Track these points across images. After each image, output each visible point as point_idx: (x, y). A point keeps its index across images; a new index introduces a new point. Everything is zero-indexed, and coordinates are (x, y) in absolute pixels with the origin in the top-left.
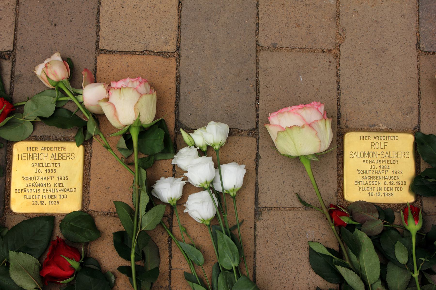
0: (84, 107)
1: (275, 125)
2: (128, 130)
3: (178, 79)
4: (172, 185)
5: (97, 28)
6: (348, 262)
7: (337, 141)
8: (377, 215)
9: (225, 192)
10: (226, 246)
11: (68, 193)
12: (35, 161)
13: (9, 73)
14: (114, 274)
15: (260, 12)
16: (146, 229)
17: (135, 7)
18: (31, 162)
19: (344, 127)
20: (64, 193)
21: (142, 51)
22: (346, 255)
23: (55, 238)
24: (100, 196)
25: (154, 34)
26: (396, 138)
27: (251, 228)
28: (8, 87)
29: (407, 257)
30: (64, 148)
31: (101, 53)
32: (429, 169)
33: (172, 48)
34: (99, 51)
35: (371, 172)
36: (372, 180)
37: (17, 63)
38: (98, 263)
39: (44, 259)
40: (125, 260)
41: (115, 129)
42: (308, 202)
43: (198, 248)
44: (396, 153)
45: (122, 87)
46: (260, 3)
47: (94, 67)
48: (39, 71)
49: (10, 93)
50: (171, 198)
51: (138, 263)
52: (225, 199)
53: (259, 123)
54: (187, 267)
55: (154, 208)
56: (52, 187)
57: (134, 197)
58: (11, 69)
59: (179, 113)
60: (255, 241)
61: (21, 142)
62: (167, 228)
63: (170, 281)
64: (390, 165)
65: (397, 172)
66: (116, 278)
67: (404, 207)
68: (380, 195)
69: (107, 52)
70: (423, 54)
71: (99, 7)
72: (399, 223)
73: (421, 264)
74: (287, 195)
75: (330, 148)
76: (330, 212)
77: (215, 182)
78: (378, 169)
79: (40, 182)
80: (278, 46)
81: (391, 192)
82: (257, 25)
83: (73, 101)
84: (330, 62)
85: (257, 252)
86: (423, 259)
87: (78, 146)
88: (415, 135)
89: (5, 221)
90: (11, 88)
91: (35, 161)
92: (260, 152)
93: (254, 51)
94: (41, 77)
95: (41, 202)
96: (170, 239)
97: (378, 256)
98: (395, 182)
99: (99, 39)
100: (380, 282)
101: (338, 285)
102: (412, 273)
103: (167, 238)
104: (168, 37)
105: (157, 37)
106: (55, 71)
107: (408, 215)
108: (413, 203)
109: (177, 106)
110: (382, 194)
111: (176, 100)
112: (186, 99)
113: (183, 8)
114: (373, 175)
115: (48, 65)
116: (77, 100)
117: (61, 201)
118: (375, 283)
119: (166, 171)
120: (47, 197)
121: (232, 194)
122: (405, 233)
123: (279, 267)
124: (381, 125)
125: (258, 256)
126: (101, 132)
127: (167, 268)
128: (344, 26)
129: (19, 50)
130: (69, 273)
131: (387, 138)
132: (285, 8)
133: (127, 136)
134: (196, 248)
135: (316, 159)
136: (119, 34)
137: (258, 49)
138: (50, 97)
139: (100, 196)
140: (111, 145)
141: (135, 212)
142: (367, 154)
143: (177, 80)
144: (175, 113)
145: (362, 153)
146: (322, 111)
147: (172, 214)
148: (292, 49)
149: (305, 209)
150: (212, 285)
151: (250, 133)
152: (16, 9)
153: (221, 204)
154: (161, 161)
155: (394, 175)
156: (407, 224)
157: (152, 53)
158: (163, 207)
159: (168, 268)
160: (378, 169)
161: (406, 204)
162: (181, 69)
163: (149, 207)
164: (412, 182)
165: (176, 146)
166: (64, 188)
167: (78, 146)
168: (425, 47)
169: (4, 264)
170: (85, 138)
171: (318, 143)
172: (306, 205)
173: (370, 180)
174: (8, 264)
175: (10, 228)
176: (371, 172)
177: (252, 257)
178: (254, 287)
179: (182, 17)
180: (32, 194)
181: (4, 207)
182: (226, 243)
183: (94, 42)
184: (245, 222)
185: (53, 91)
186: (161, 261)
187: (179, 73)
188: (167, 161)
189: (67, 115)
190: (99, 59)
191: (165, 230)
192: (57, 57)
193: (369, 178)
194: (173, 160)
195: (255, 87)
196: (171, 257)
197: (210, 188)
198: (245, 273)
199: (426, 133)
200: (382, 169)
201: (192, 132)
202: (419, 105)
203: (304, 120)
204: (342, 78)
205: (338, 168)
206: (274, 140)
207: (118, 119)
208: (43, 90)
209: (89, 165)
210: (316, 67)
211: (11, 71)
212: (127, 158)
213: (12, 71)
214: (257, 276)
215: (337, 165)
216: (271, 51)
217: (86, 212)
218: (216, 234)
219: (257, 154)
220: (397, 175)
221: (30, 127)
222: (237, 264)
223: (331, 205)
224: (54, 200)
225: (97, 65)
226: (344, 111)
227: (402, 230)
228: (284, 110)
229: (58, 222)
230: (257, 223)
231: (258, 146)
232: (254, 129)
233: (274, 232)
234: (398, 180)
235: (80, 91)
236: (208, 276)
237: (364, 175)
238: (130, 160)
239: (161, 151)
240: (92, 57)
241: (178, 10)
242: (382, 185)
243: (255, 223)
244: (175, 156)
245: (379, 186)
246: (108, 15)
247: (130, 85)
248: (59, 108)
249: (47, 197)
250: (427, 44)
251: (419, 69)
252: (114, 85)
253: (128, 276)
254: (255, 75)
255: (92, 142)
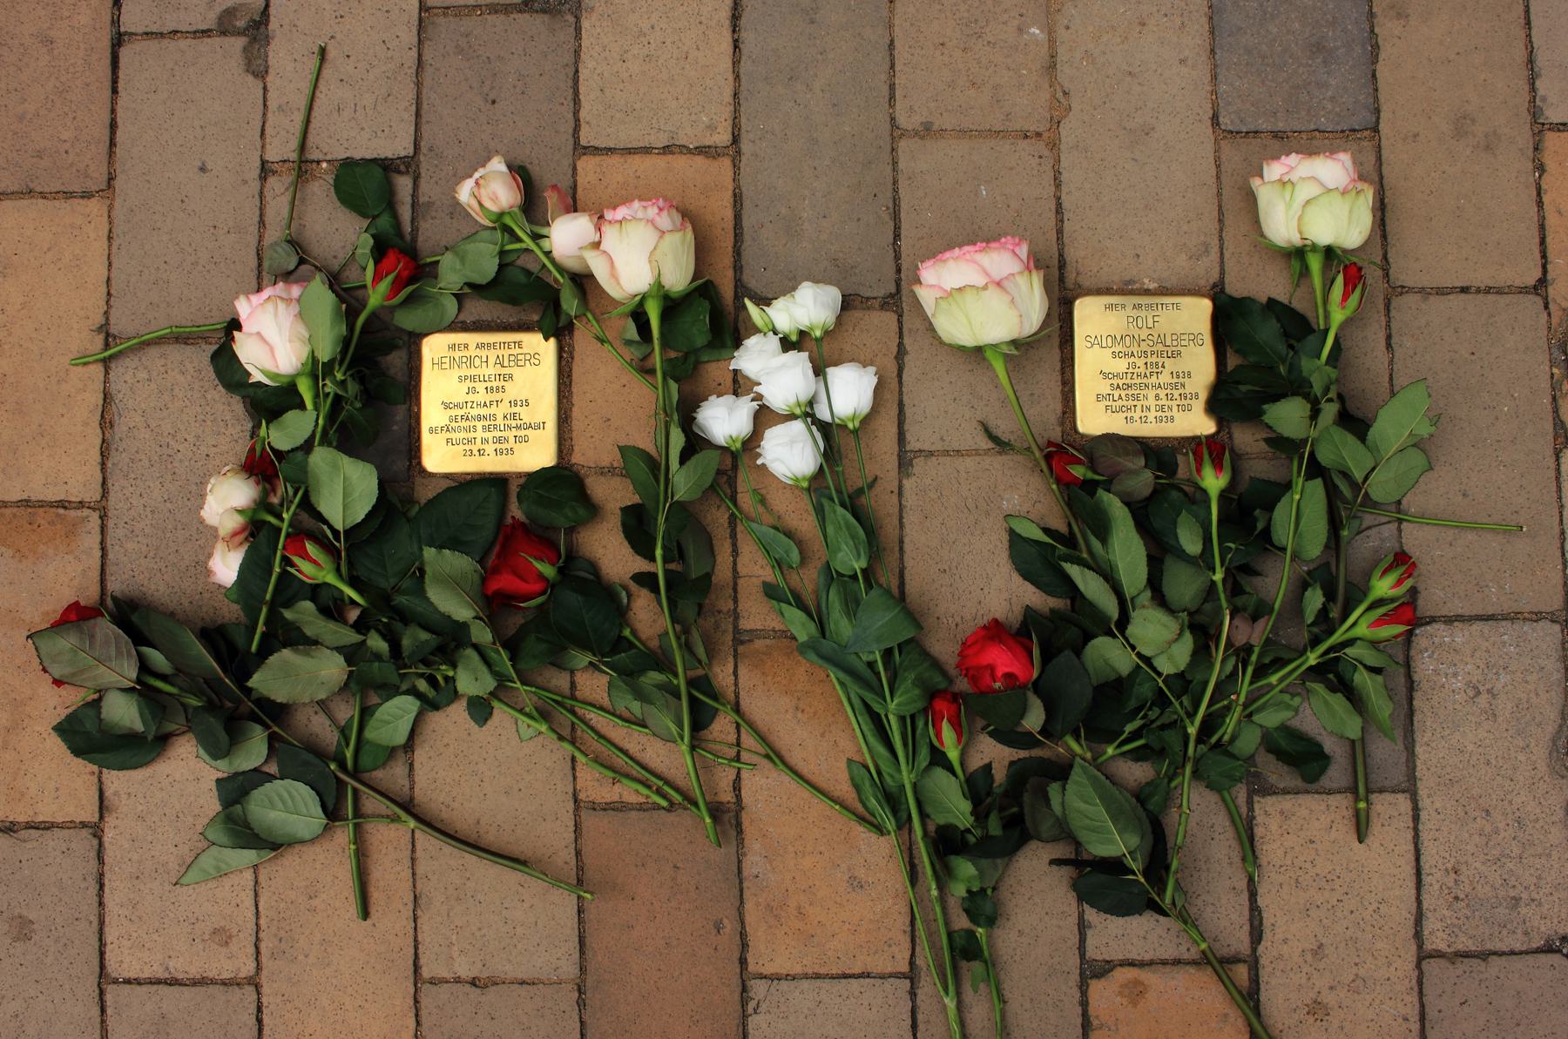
0: (553, 261)
1: (931, 286)
2: (641, 303)
3: (737, 199)
4: (731, 410)
5: (575, 104)
6: (1085, 555)
7: (1060, 315)
8: (1142, 462)
9: (837, 421)
10: (841, 528)
11: (529, 432)
12: (465, 371)
13: (409, 200)
14: (625, 588)
15: (897, 62)
16: (682, 499)
17: (647, 59)
18: (456, 373)
19: (1072, 287)
20: (522, 433)
21: (664, 148)
22: (1081, 541)
23: (509, 521)
24: (592, 437)
25: (687, 112)
26: (1177, 306)
27: (892, 492)
28: (407, 228)
29: (1201, 543)
30: (519, 344)
31: (584, 154)
32: (1241, 365)
33: (722, 137)
34: (580, 150)
35: (1129, 376)
36: (1130, 392)
37: (422, 180)
38: (594, 568)
39: (490, 562)
40: (647, 562)
41: (615, 303)
42: (1004, 438)
43: (789, 534)
44: (1177, 337)
45: (624, 217)
46: (896, 43)
47: (571, 183)
48: (464, 193)
49: (412, 239)
50: (731, 437)
51: (672, 566)
52: (839, 438)
53: (903, 283)
54: (768, 570)
55: (697, 456)
56: (500, 421)
57: (658, 437)
58: (411, 192)
59: (742, 267)
60: (901, 518)
61: (437, 335)
62: (725, 495)
63: (736, 601)
64: (1166, 360)
65: (1181, 375)
66: (629, 595)
67: (1195, 444)
68: (1148, 421)
69: (596, 151)
70: (1225, 137)
71: (576, 63)
72: (1185, 477)
73: (1230, 556)
74: (963, 425)
75: (1042, 328)
76: (1048, 458)
77: (817, 403)
78: (1142, 370)
79: (475, 412)
80: (935, 127)
81: (1169, 414)
82: (892, 87)
83: (532, 251)
84: (1040, 157)
85: (906, 540)
86: (1232, 545)
87: (546, 339)
88: (1214, 300)
89: (413, 489)
90: (412, 230)
91: (465, 371)
92: (907, 341)
93: (888, 139)
94: (469, 206)
95: (479, 451)
96: (732, 516)
97: (1142, 542)
98: (1176, 394)
99: (580, 126)
100: (1148, 594)
101: (1069, 602)
102: (1211, 573)
103: (727, 516)
104: (714, 117)
105: (693, 117)
106: (494, 193)
107: (1202, 460)
108: (1213, 435)
109: (737, 253)
110: (1151, 418)
111: (736, 242)
112: (754, 240)
113: (744, 58)
114: (1133, 382)
115: (481, 182)
116: (541, 248)
117: (517, 447)
118: (1139, 594)
119: (720, 384)
120: (490, 441)
121: (851, 426)
122: (1198, 495)
123: (950, 569)
124: (1146, 281)
125: (907, 547)
126: (587, 309)
127: (729, 574)
128: (1067, 86)
129: (425, 155)
130: (538, 587)
131: (1160, 306)
132: (946, 52)
133: (639, 316)
134: (785, 534)
135: (1015, 352)
136: (618, 115)
137: (895, 134)
138: (488, 245)
139: (592, 437)
140: (610, 335)
141: (660, 464)
142: (1119, 338)
143: (735, 201)
144: (734, 267)
145: (1109, 338)
146: (1024, 255)
147: (735, 467)
148: (963, 133)
149: (1000, 453)
150: (818, 607)
151: (885, 303)
152: (417, 74)
153: (830, 446)
154: (709, 364)
155: (1175, 380)
156: (1200, 476)
157: (684, 150)
158: (715, 454)
159: (731, 575)
160: (1142, 370)
161: (1199, 437)
162: (745, 180)
163: (685, 457)
164: (1209, 393)
165: (739, 334)
166: (522, 422)
167: (546, 339)
168: (1228, 122)
169: (414, 572)
170: (558, 321)
171: (1016, 320)
172: (1000, 445)
173: (1126, 392)
174: (422, 571)
175: (423, 501)
176: (1129, 376)
177: (897, 549)
178: (899, 608)
179: (742, 76)
180: (462, 435)
181: (411, 462)
182: (842, 522)
183: (571, 131)
184: (879, 481)
185: (494, 232)
186: (718, 562)
187: (739, 187)
188: (722, 364)
189: (522, 279)
190: (580, 164)
191: (722, 499)
192: (497, 165)
193: (1125, 387)
194: (733, 361)
195: (891, 210)
196: (735, 552)
197: (807, 415)
198: (883, 580)
199: (1237, 295)
200: (1150, 370)
201: (768, 305)
202: (1221, 239)
203: (987, 274)
204: (1064, 189)
205: (1062, 369)
206: (930, 316)
207: (619, 284)
208: (473, 231)
209: (570, 376)
210: (1011, 169)
211: (413, 196)
212: (642, 360)
213: (415, 195)
214: (907, 587)
215: (1059, 364)
216: (922, 138)
217: (566, 468)
218: (822, 506)
219: (900, 345)
220: (1181, 380)
221: (451, 306)
222: (863, 563)
223: (1050, 444)
224: (504, 446)
225: (578, 178)
226: (1071, 254)
227: (1193, 489)
228: (948, 255)
229: (514, 489)
230: (905, 482)
231: (901, 329)
232: (892, 296)
233: (939, 498)
234: (1182, 391)
235: (544, 231)
236: (810, 590)
237: (1115, 382)
238: (648, 364)
239: (706, 343)
240: (567, 162)
241: (734, 63)
242: (1151, 402)
243: (900, 481)
244: (735, 354)
245: (1145, 403)
246: (596, 77)
247: (640, 215)
248: (507, 265)
249: (490, 441)
250: (1232, 117)
251: (1218, 167)
252: (609, 215)
253: (652, 591)
254: (890, 187)
255: (573, 330)
